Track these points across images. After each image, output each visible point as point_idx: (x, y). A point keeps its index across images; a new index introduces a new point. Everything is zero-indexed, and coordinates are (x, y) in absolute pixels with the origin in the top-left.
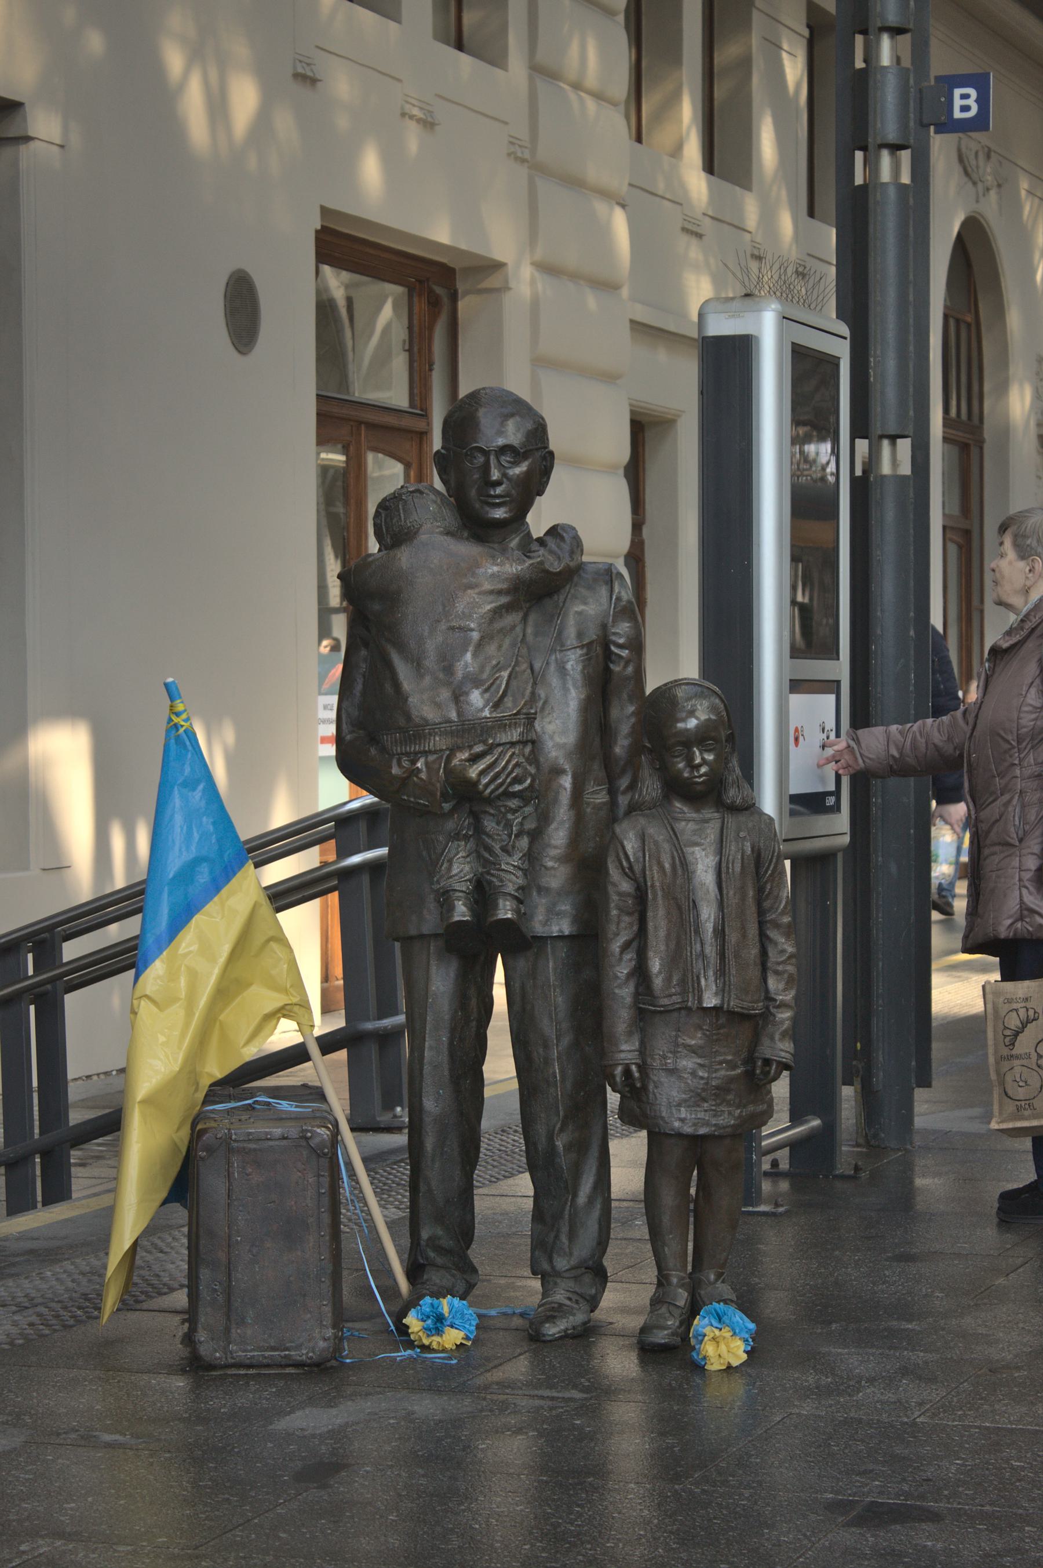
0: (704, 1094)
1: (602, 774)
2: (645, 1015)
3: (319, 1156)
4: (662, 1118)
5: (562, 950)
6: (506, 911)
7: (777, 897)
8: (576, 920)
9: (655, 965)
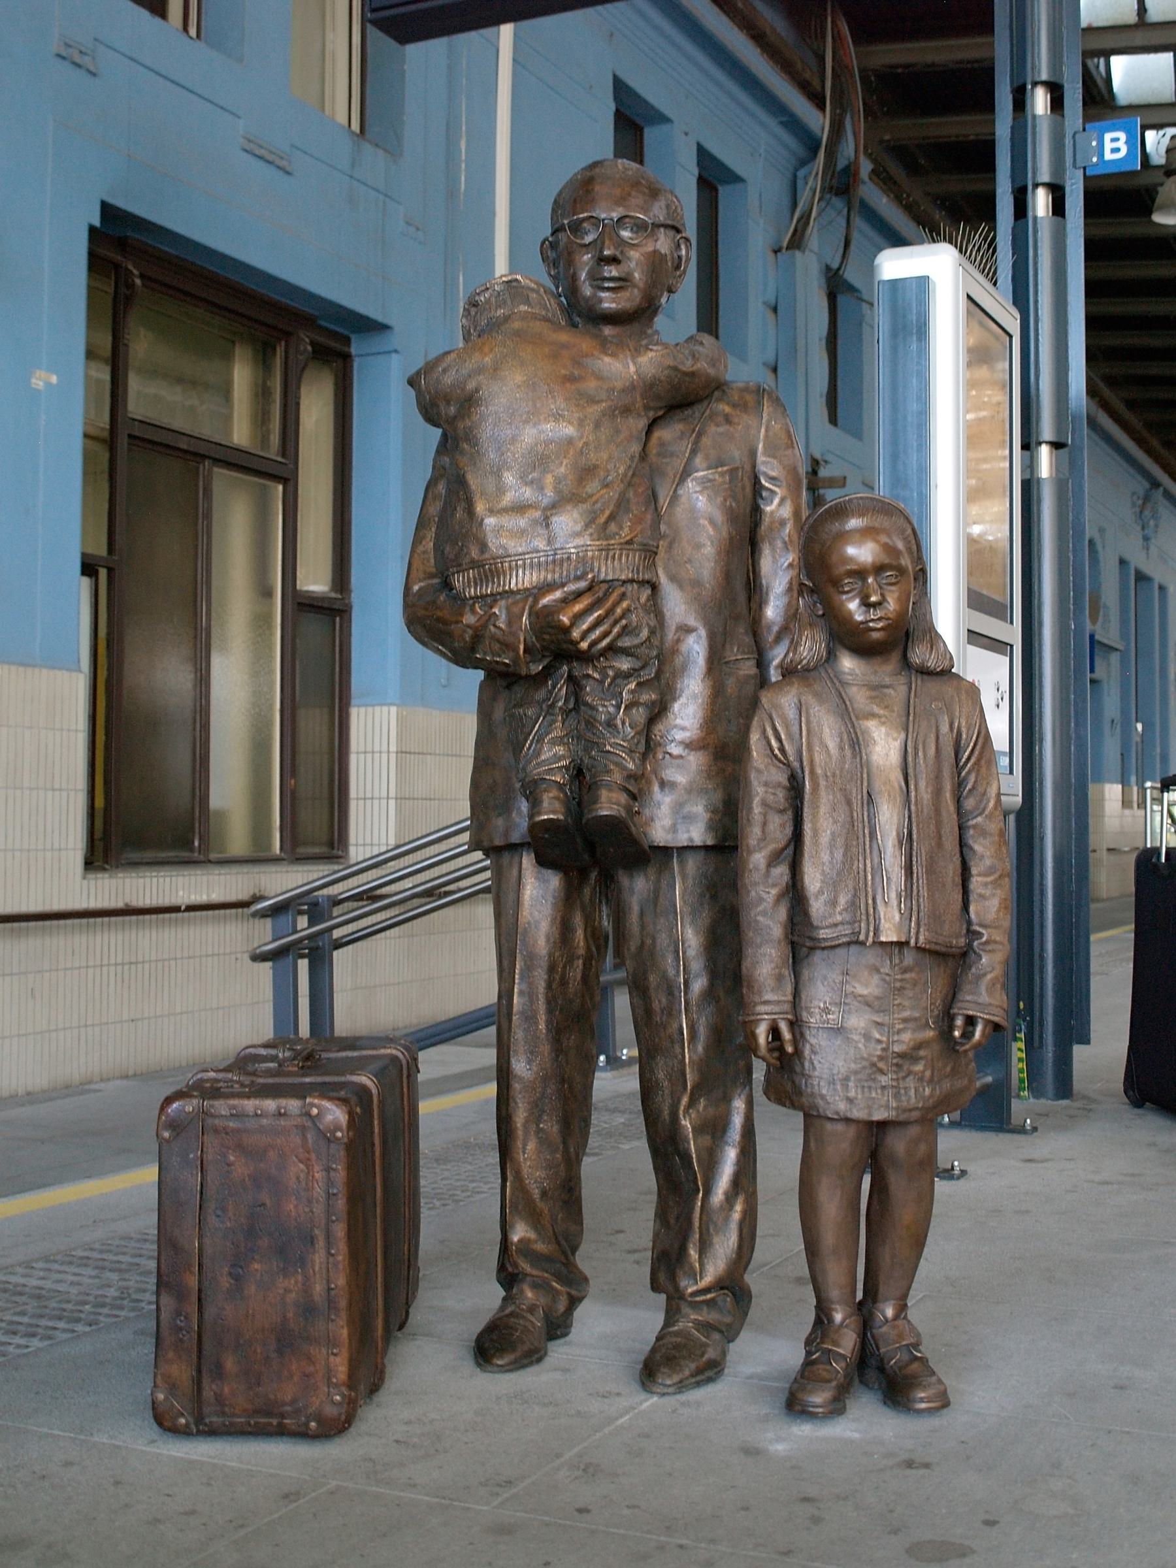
0: (881, 1065)
1: (748, 640)
2: (801, 942)
3: (329, 1140)
4: (823, 1097)
5: (693, 864)
6: (609, 804)
7: (984, 794)
8: (712, 827)
9: (813, 880)
